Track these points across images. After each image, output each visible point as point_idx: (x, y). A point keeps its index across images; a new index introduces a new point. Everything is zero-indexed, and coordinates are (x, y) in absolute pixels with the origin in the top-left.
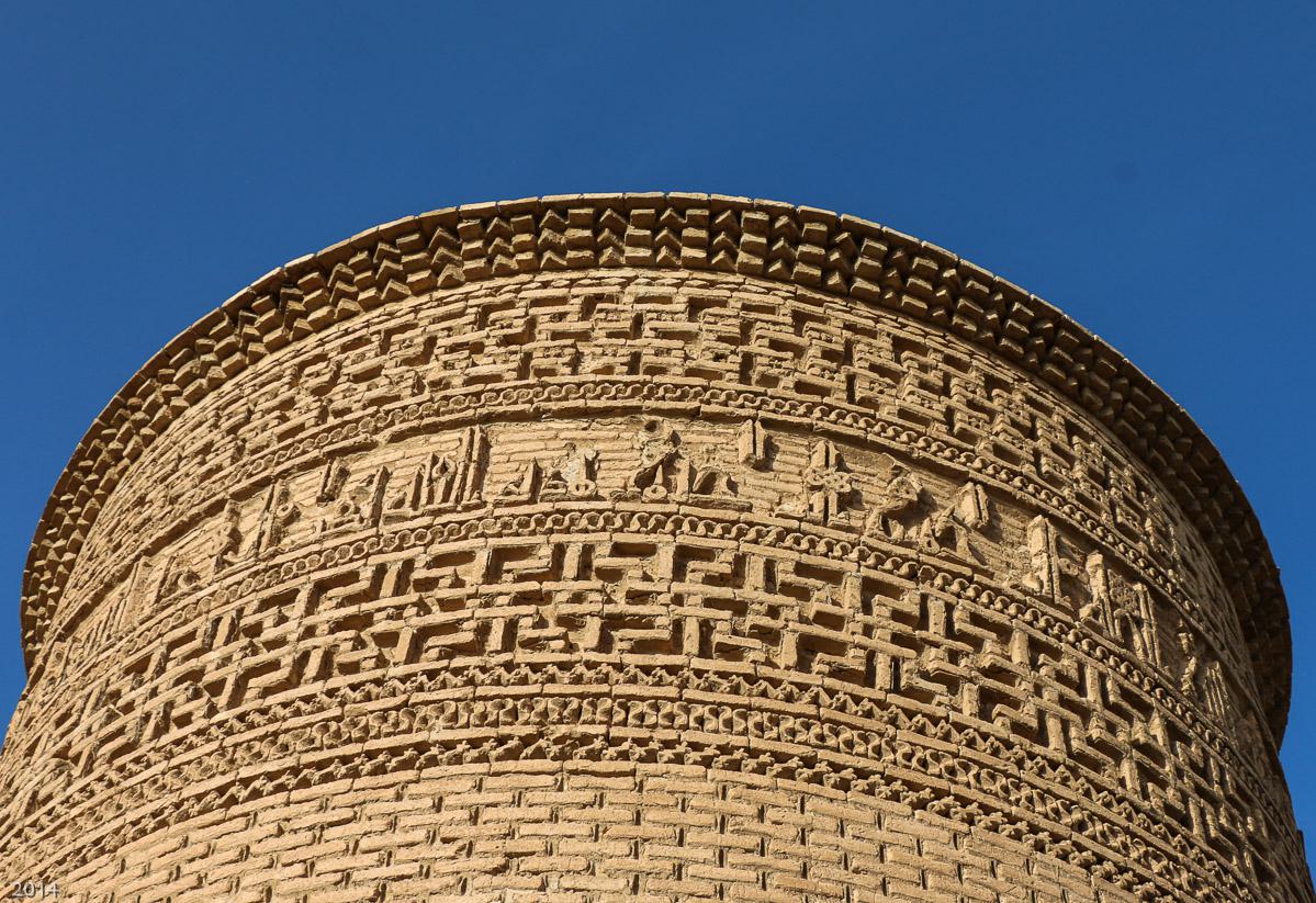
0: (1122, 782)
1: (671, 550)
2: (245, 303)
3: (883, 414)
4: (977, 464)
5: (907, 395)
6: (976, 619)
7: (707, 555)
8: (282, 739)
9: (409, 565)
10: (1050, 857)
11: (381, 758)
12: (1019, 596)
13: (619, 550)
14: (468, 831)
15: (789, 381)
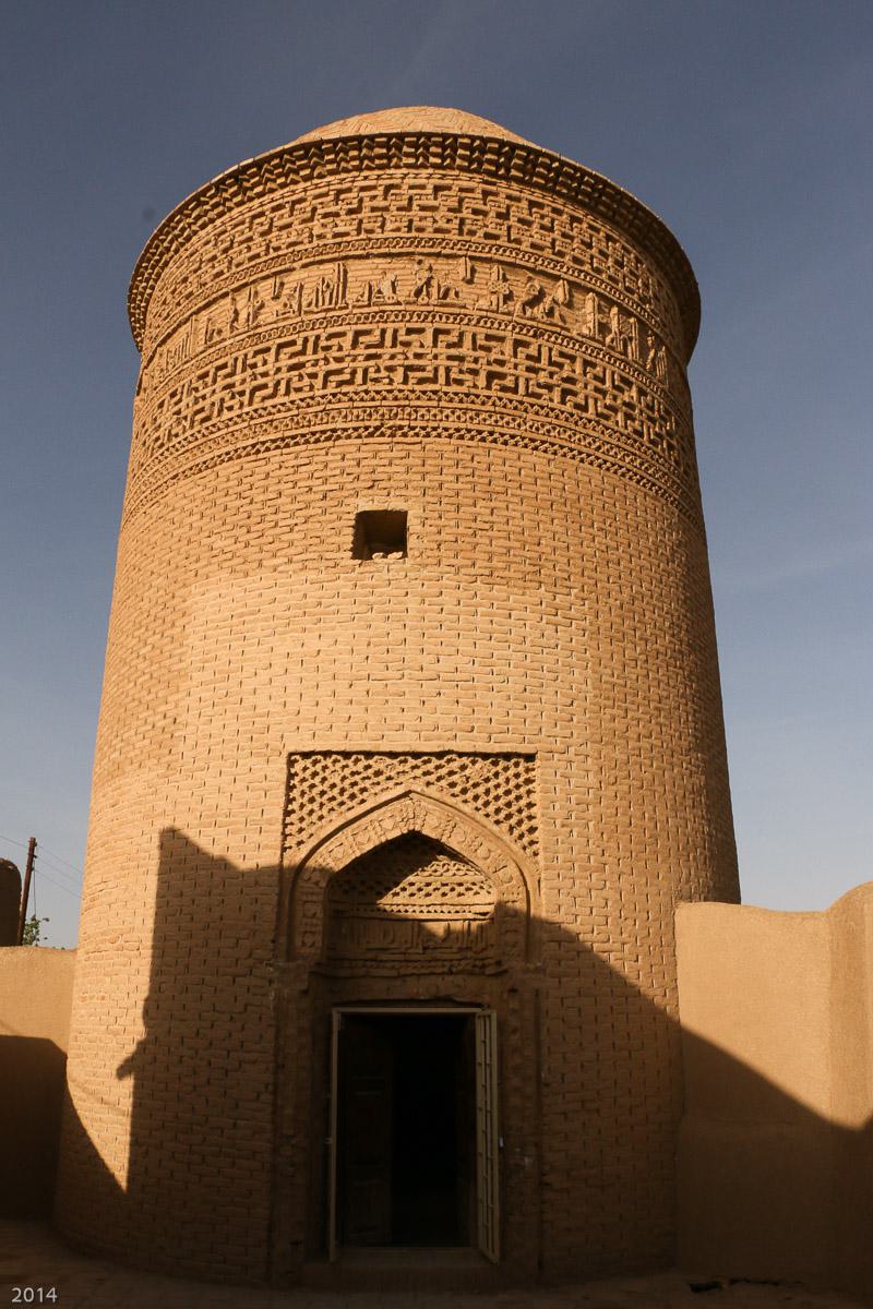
0: (617, 423)
1: (432, 330)
2: (222, 181)
3: (523, 247)
4: (565, 269)
5: (536, 236)
6: (562, 354)
7: (447, 332)
8: (275, 423)
9: (318, 337)
10: (586, 465)
11: (318, 435)
12: (580, 339)
13: (409, 331)
14: (357, 470)
15: (481, 233)
